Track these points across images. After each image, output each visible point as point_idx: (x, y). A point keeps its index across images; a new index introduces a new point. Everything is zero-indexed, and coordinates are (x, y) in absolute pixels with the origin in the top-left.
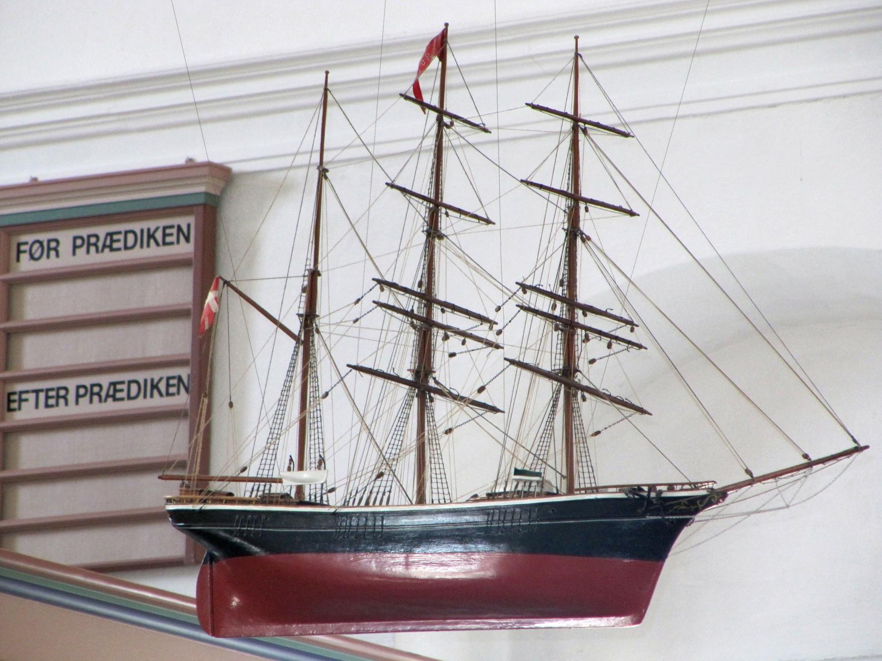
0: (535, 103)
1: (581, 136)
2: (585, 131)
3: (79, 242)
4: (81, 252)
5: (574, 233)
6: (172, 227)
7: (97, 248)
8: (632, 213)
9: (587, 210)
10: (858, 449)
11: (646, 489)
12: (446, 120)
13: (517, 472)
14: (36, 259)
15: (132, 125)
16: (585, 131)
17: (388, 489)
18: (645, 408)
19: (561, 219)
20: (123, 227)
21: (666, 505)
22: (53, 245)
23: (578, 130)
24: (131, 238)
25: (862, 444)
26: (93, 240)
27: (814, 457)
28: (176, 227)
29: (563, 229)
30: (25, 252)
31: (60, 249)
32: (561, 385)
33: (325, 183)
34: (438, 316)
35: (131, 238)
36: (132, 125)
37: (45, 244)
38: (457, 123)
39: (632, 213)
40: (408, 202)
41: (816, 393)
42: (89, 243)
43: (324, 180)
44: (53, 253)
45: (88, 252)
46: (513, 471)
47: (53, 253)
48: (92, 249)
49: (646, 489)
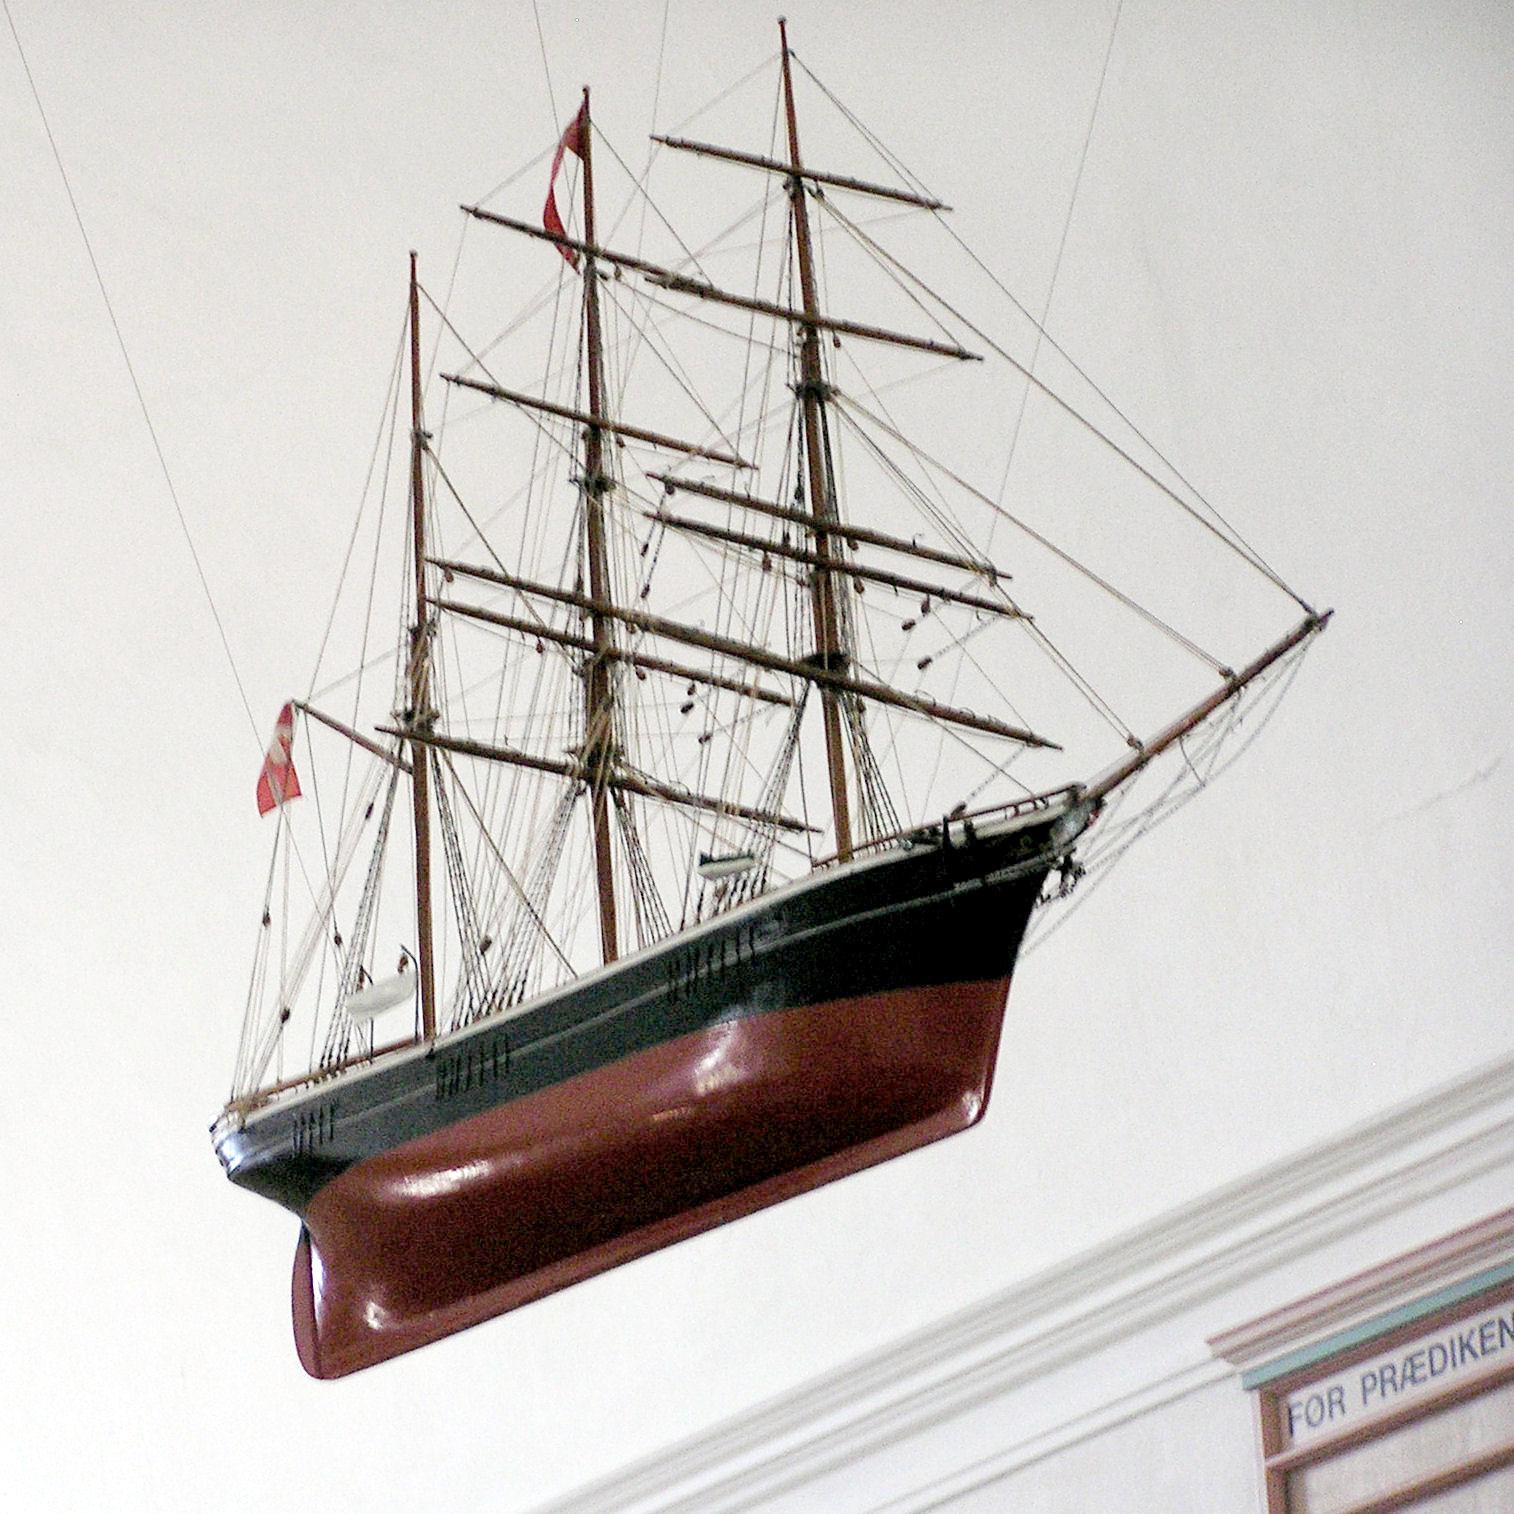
0: (676, 137)
1: (810, 203)
2: (819, 195)
3: (1369, 1382)
4: (1374, 1396)
5: (813, 393)
6: (1491, 1323)
7: (1394, 1385)
8: (963, 356)
9: (837, 344)
10: (1314, 623)
11: (927, 831)
12: (601, 265)
13: (705, 860)
14: (1314, 1425)
15: (1425, 1185)
16: (819, 195)
17: (522, 978)
18: (1039, 733)
19: (787, 371)
20: (1423, 1344)
21: (985, 851)
22: (1336, 1396)
23: (803, 195)
24: (1438, 1356)
25: (1320, 611)
26: (1388, 1374)
27: (1238, 671)
28: (1497, 1323)
29: (788, 385)
30: (1299, 1417)
31: (1346, 1402)
32: (808, 683)
33: (426, 460)
34: (622, 639)
35: (1438, 1356)
36: (1425, 1185)
37: (1325, 1398)
38: (629, 275)
39: (963, 356)
40: (536, 428)
41: (1231, 538)
42: (1382, 1381)
43: (423, 452)
44: (1337, 1409)
45: (1383, 1393)
46: (697, 861)
47: (1337, 1409)
48: (1389, 1387)
49: (927, 831)
